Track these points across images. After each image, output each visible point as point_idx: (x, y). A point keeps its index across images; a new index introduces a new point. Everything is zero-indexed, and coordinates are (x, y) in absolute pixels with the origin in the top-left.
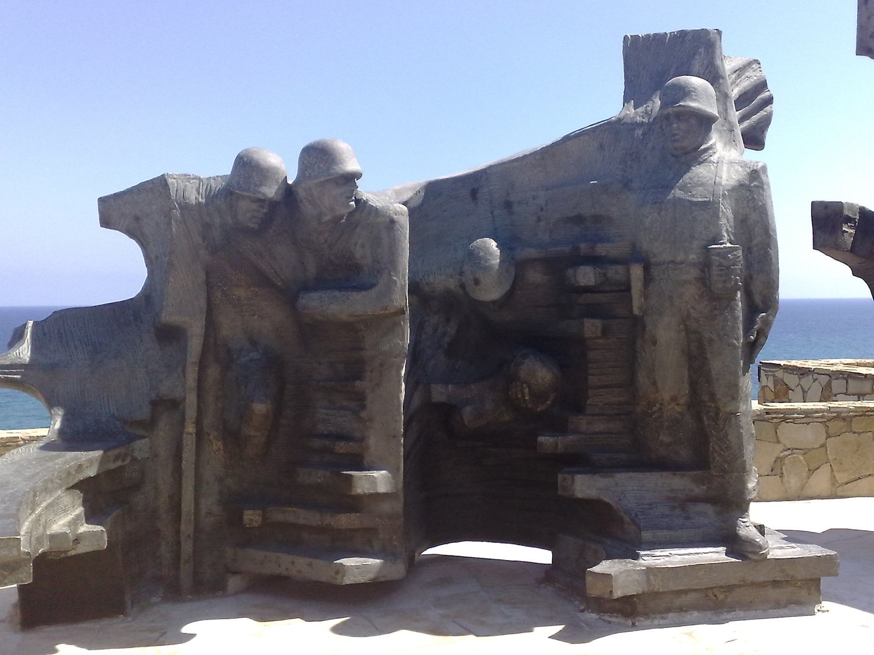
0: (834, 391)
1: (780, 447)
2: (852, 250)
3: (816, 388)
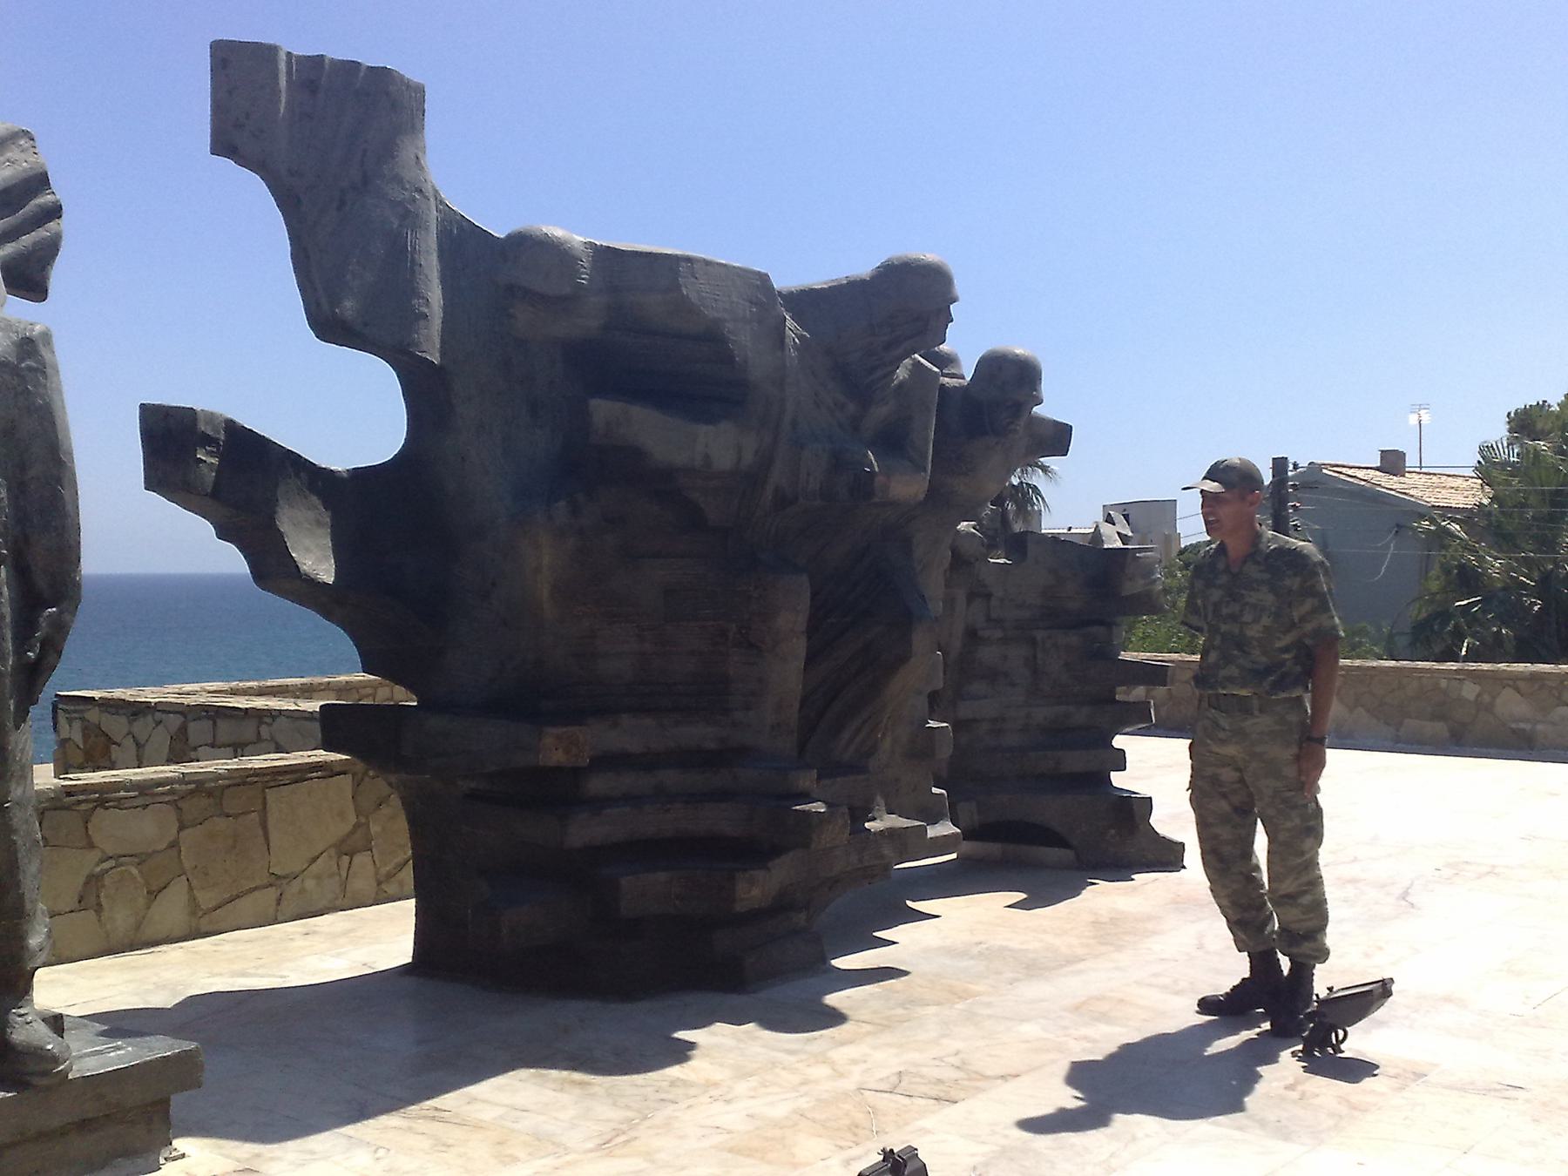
0: (192, 741)
1: (94, 856)
2: (215, 494)
3: (160, 740)
